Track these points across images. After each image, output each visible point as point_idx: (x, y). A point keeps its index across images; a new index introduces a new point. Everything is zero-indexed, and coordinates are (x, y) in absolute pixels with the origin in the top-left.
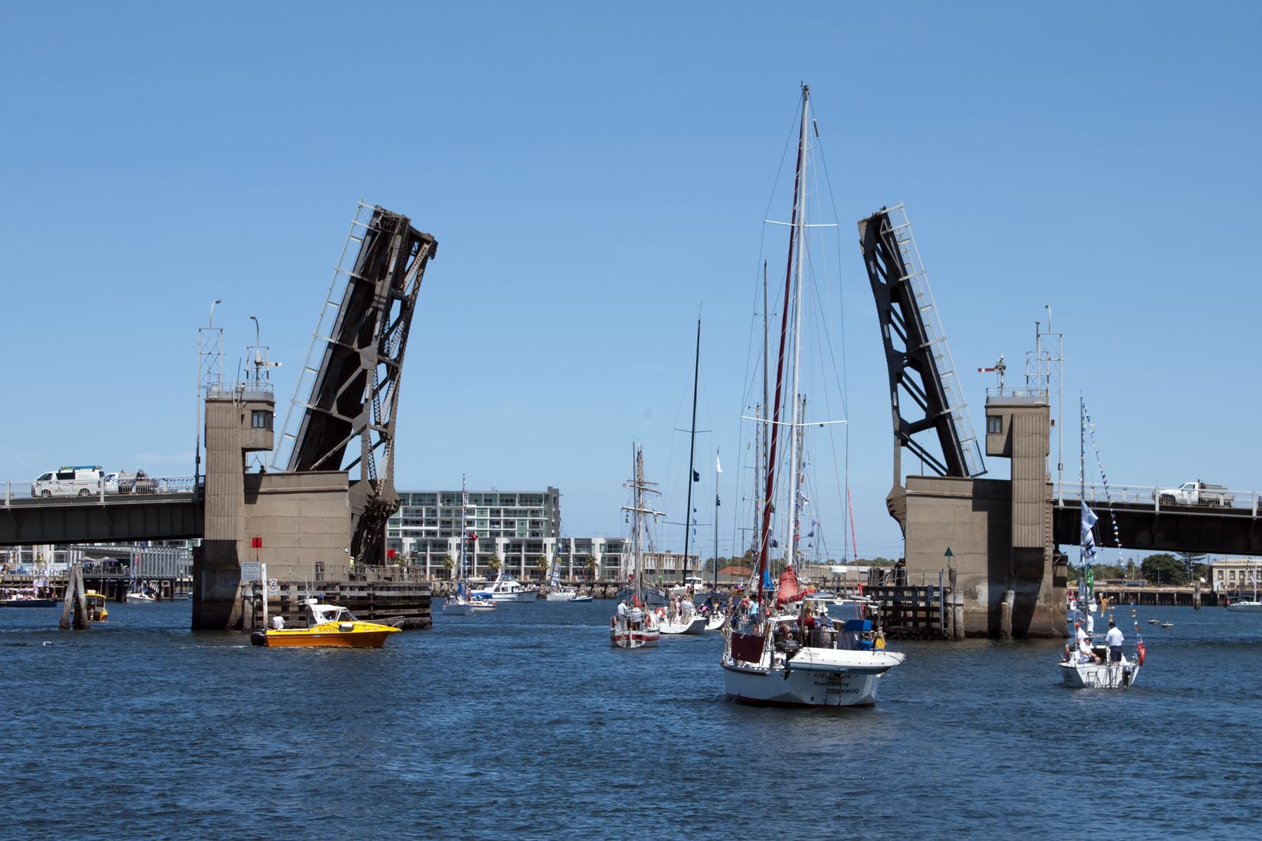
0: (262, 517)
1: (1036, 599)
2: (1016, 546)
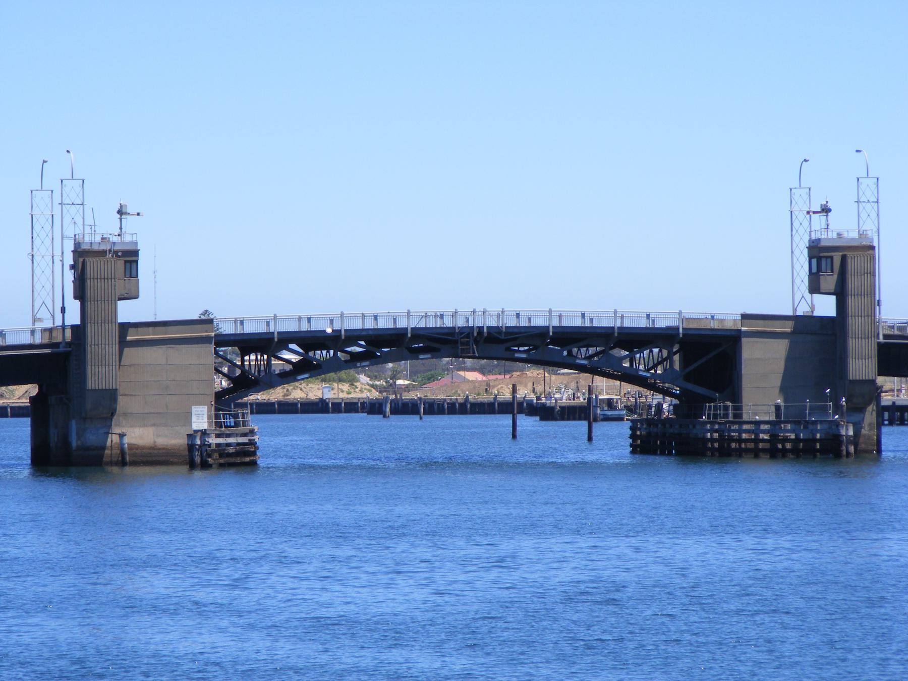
0: (130, 366)
1: (861, 428)
2: (851, 378)
